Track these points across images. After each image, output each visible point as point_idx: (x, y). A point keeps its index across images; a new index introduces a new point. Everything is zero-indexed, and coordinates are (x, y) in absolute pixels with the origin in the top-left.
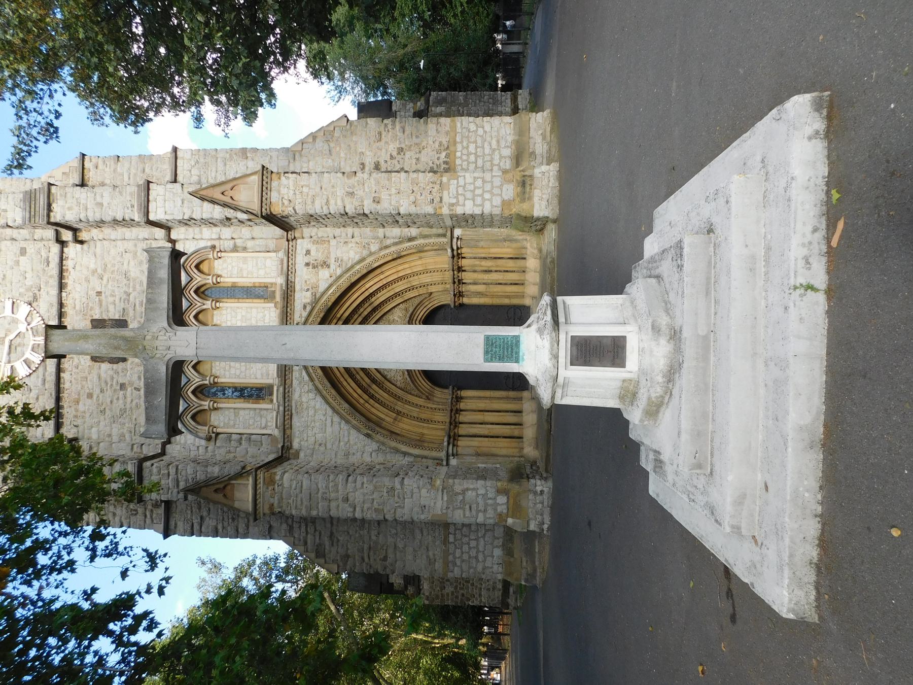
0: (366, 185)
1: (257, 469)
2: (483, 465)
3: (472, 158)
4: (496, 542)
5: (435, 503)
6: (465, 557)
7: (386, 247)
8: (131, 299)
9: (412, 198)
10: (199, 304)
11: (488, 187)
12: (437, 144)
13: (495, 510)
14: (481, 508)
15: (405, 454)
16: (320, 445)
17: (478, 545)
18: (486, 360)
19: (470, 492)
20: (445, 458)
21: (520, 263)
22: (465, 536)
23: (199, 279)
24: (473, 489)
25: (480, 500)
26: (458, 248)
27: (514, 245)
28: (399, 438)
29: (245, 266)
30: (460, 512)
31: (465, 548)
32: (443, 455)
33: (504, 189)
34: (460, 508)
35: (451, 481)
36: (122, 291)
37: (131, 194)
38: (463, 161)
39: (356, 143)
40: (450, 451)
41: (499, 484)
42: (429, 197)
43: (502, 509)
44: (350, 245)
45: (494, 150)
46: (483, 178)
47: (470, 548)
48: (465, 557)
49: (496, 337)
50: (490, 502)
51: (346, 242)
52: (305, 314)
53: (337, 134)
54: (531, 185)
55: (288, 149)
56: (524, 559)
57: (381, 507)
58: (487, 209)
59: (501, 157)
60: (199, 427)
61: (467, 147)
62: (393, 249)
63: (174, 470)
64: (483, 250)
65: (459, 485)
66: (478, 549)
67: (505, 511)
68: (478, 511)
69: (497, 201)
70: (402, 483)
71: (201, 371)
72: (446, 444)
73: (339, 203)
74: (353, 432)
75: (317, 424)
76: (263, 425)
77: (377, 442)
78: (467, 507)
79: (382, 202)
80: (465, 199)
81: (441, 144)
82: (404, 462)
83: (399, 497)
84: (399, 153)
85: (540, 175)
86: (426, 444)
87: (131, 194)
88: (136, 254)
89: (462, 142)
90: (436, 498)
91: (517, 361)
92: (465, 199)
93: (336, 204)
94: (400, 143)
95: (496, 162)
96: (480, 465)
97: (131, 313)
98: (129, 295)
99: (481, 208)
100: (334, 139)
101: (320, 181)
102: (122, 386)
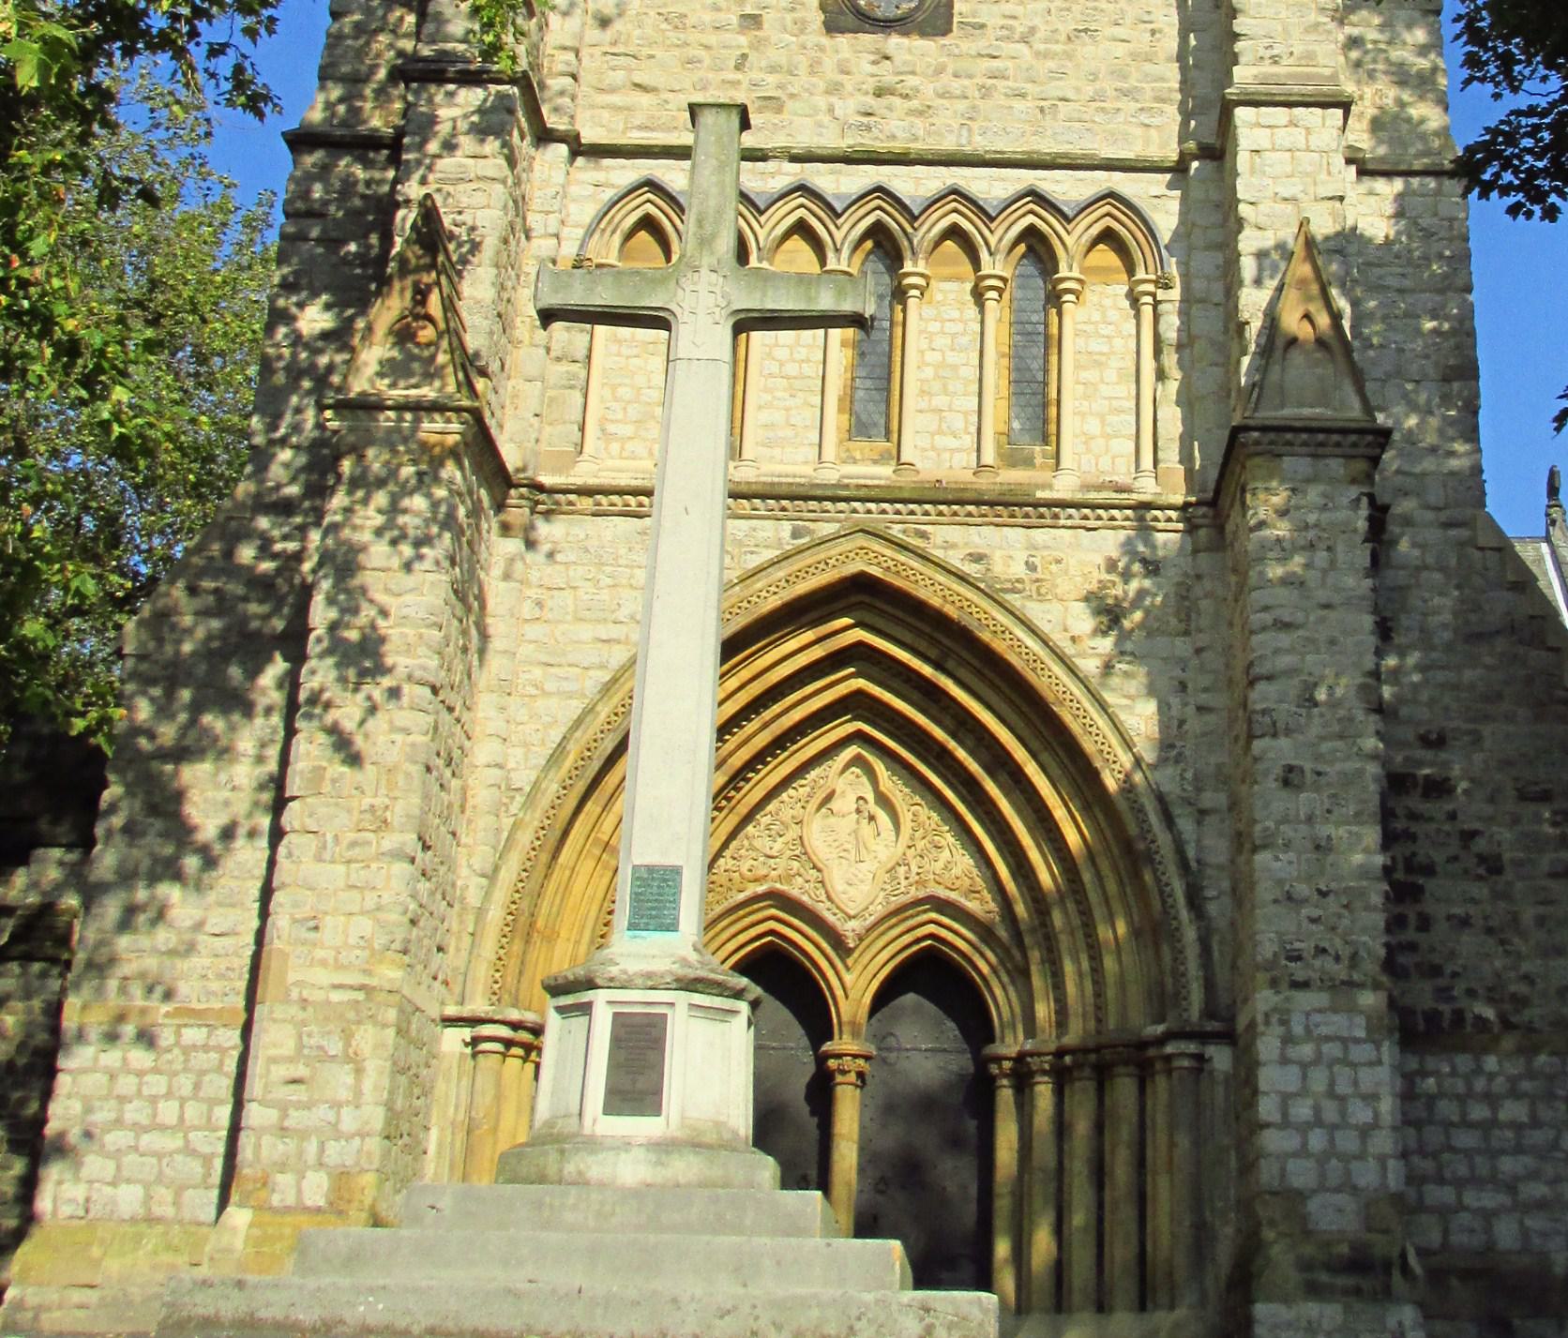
0: (1339, 744)
1: (477, 415)
2: (432, 1149)
3: (1479, 1112)
4: (165, 1194)
5: (324, 963)
6: (127, 1084)
7: (1169, 820)
8: (1009, 48)
9: (1303, 889)
10: (993, 240)
11: (1347, 1142)
12: (1522, 989)
13: (282, 1167)
14: (296, 1118)
15: (492, 876)
16: (539, 604)
17: (163, 1128)
18: (672, 927)
19: (350, 1080)
20: (466, 1011)
21: (1124, 1287)
22: (197, 1086)
23: (1069, 240)
24: (358, 1092)
25: (323, 1113)
26: (1168, 1058)
27: (1181, 1261)
28: (544, 857)
29: (1111, 375)
30: (289, 1047)
31: (157, 1084)
32: (478, 1006)
33: (1342, 1199)
34: (300, 1046)
35: (392, 1015)
36: (1037, 21)
37: (1309, 57)
38: (1468, 1079)
39: (1509, 718)
40: (487, 1030)
41: (370, 1179)
42: (1306, 947)
43: (284, 1190)
44: (1175, 701)
45: (1511, 1188)
46: (1375, 1125)
47: (153, 1100)
48: (127, 1084)
49: (677, 893)
50: (312, 1147)
51: (1183, 686)
52: (955, 559)
53: (1537, 657)
54: (1358, 1292)
55: (1480, 501)
56: (92, 1296)
57: (327, 787)
58: (1273, 1141)
59: (1488, 1216)
60: (617, 239)
61: (1514, 1094)
62: (1163, 839)
63: (491, 174)
64: (1163, 1148)
65: (373, 1041)
66: (146, 1130)
67: (276, 1200)
68: (284, 1109)
69: (1301, 1175)
70: (397, 855)
71: (789, 244)
72: (514, 1015)
73: (1285, 661)
74: (576, 707)
75: (605, 595)
76: (611, 428)
77: (536, 785)
78: (301, 1071)
79: (1284, 794)
80: (1304, 1066)
81: (1521, 1002)
82: (464, 872)
83: (353, 844)
84: (1482, 859)
85: (1391, 1322)
86: (517, 947)
87: (1309, 57)
88: (1149, 59)
89: (1531, 1074)
90: (339, 967)
91: (633, 926)
92: (1304, 1066)
93: (1277, 651)
94: (1518, 864)
95: (1470, 1198)
96: (434, 1134)
97: (968, 46)
98: (1024, 40)
99: (1276, 1117)
100: (1521, 650)
101: (1347, 603)
102: (752, 21)
